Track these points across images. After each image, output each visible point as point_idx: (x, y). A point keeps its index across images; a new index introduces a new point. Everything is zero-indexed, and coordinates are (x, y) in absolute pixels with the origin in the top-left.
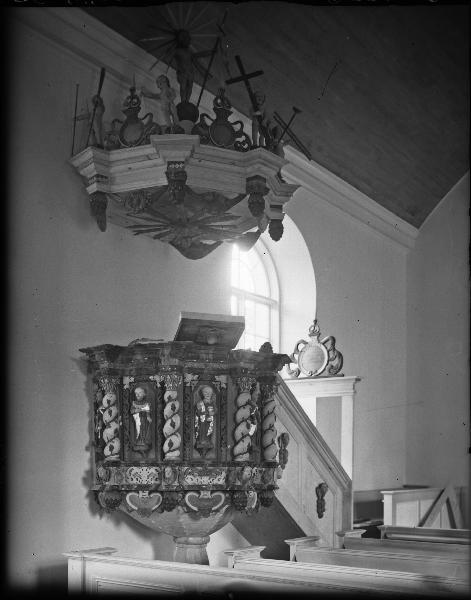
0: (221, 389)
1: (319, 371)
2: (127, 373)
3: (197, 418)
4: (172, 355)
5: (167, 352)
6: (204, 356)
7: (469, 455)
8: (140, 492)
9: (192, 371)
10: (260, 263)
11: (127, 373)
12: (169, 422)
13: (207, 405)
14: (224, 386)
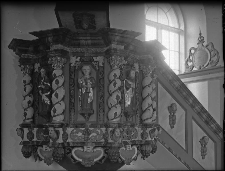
0: (99, 67)
1: (205, 66)
3: (80, 90)
4: (56, 42)
5: (50, 39)
6: (83, 42)
7: (223, 90)
8: (44, 146)
9: (75, 54)
12: (60, 85)
14: (101, 65)
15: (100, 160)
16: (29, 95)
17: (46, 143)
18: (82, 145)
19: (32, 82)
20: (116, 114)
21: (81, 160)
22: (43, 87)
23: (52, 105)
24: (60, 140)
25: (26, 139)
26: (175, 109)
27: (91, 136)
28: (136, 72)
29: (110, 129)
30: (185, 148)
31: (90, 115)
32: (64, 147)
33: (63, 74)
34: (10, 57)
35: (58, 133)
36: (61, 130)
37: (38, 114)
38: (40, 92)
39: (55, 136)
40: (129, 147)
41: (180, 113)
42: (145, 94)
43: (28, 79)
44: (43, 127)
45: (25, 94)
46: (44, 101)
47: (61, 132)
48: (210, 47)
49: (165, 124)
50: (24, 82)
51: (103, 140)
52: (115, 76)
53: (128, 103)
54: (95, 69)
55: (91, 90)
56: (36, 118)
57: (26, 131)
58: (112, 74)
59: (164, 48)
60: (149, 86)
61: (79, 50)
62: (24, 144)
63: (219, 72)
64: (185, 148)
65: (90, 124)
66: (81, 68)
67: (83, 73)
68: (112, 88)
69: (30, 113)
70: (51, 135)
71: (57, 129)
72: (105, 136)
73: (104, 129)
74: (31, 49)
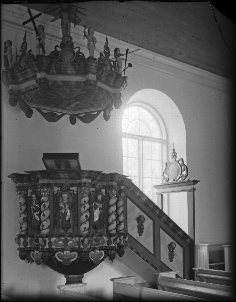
1: (177, 178)
2: (29, 188)
4: (43, 178)
8: (35, 251)
9: (57, 185)
10: (138, 134)
11: (29, 188)
12: (46, 208)
13: (64, 204)
15: (75, 261)
16: (24, 213)
17: (37, 248)
19: (26, 203)
20: (85, 228)
21: (61, 261)
22: (34, 208)
23: (40, 222)
24: (47, 247)
25: (22, 246)
26: (142, 220)
27: (69, 243)
28: (103, 196)
30: (153, 253)
31: (68, 228)
32: (50, 252)
33: (48, 200)
34: (8, 185)
35: (45, 241)
36: (47, 239)
37: (31, 227)
38: (32, 211)
39: (43, 244)
40: (98, 252)
41: (148, 223)
43: (22, 201)
44: (34, 237)
45: (20, 212)
46: (35, 218)
47: (48, 241)
48: (180, 162)
49: (133, 232)
50: (20, 203)
51: (77, 246)
52: (85, 201)
53: (96, 219)
54: (72, 196)
55: (68, 211)
56: (29, 231)
57: (22, 240)
58: (83, 200)
59: (127, 176)
60: (113, 205)
61: (59, 182)
62: (21, 250)
63: (189, 185)
64: (153, 253)
65: (67, 235)
66: (61, 194)
67: (62, 198)
68: (82, 209)
69: (24, 226)
70: (41, 243)
71: (44, 239)
73: (77, 238)
74: (25, 179)
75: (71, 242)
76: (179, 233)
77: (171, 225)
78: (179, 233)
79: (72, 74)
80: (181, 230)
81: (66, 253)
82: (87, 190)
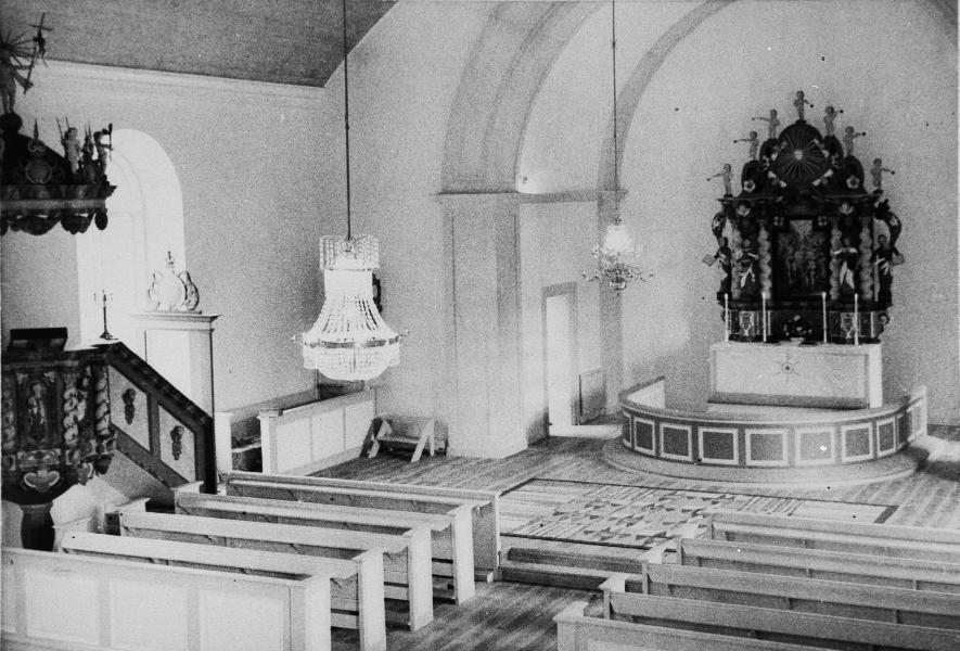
13: (38, 401)
15: (56, 484)
18: (35, 470)
21: (34, 486)
29: (68, 452)
30: (148, 449)
41: (140, 399)
42: (99, 401)
48: (184, 277)
49: (119, 418)
64: (148, 449)
72: (61, 458)
73: (58, 451)
75: (47, 457)
76: (189, 409)
77: (155, 380)
78: (189, 409)
79: (45, 199)
80: (192, 403)
81: (43, 473)
82: (70, 378)
